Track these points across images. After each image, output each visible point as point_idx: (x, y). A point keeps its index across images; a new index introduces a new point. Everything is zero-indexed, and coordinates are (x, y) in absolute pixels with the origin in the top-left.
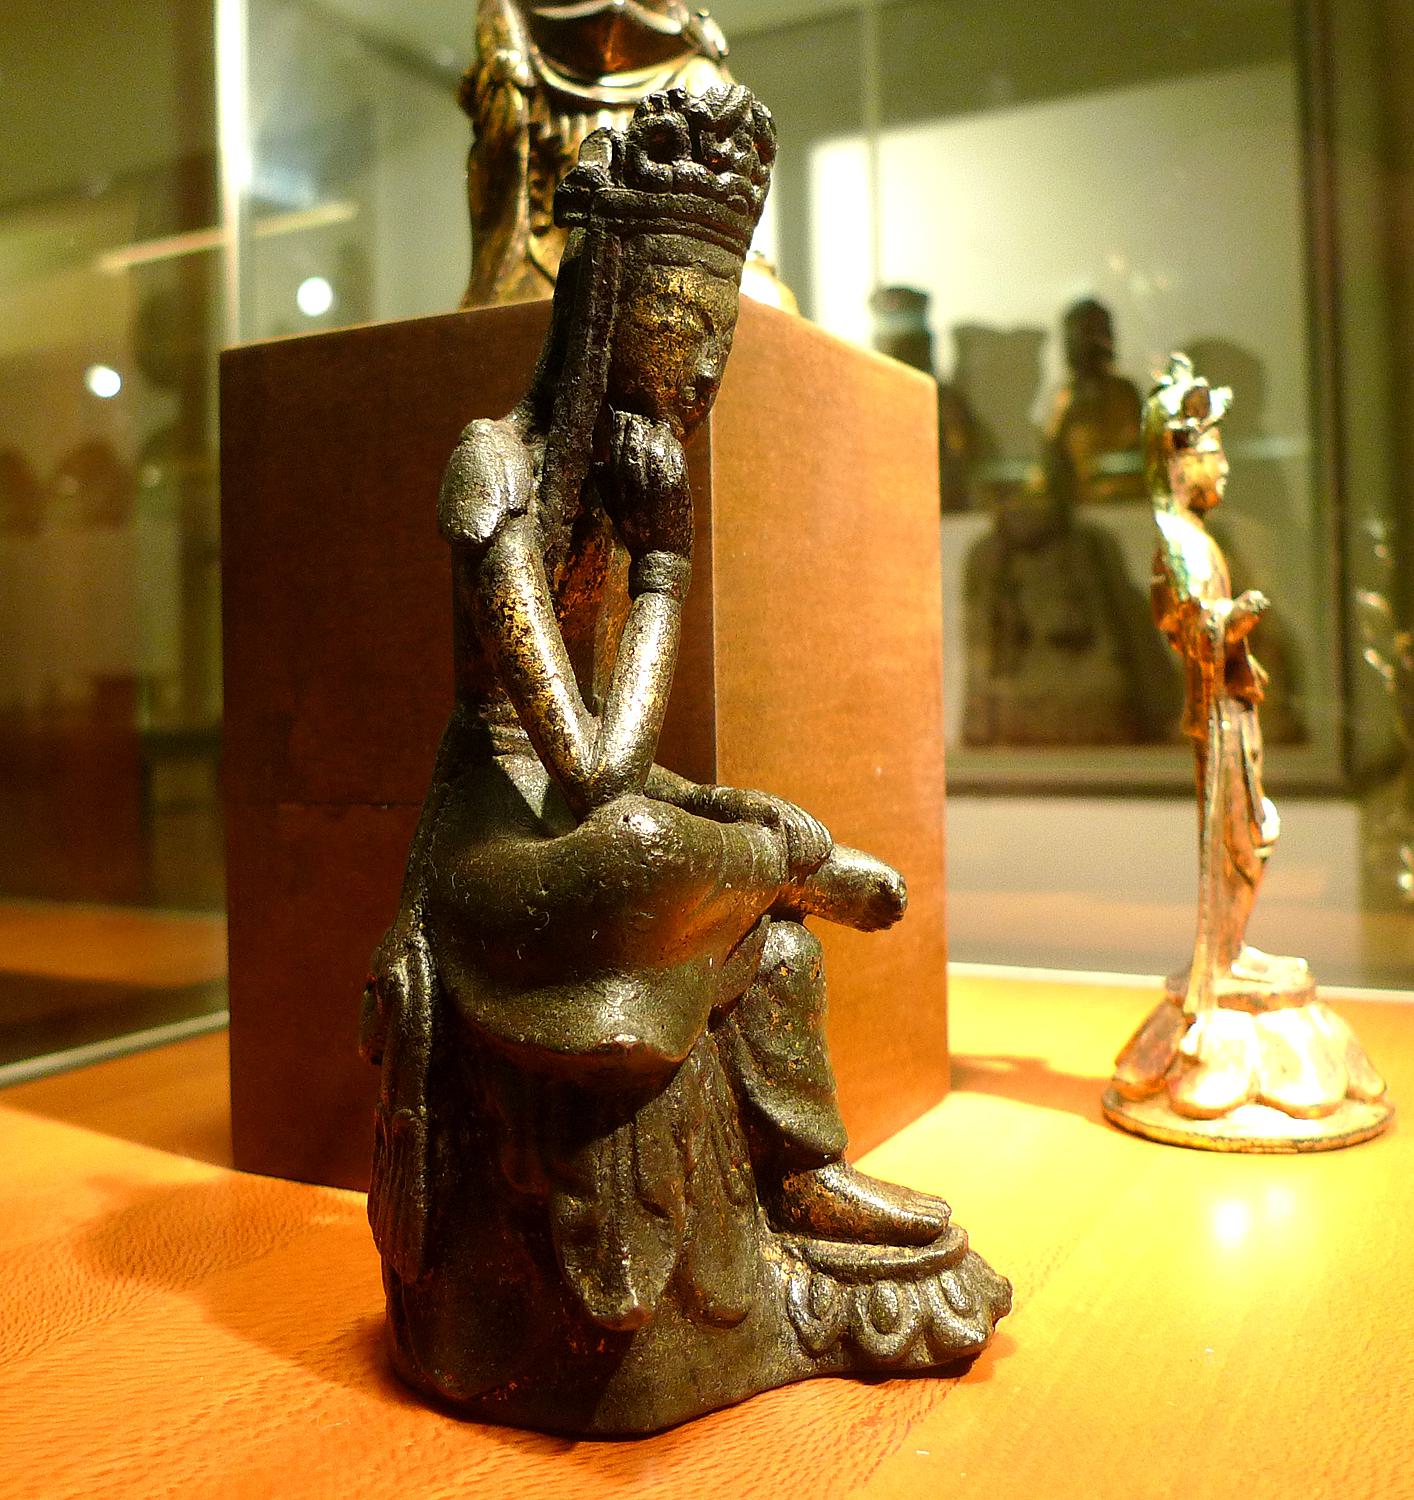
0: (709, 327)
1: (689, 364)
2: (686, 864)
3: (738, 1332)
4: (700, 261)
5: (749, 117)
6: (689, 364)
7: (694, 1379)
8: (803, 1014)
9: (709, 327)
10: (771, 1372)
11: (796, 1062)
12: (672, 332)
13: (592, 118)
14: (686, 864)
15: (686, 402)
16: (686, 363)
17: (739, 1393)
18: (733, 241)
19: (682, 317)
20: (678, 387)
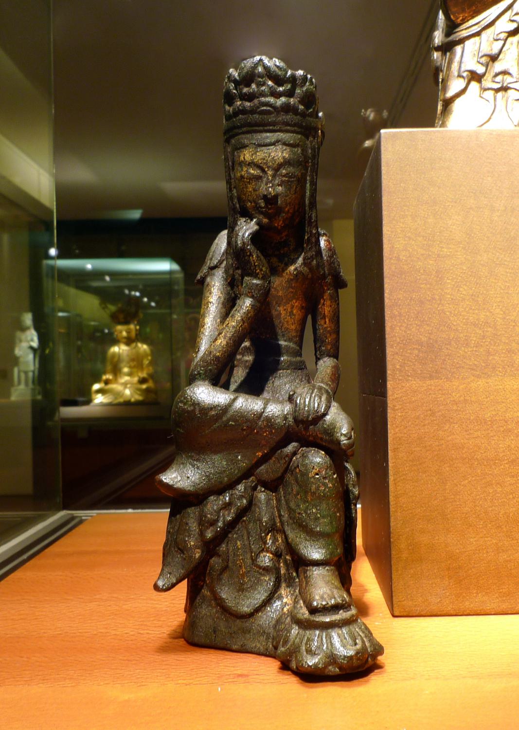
0: (263, 170)
1: (256, 190)
2: (194, 411)
3: (242, 622)
4: (252, 143)
5: (260, 69)
6: (256, 190)
7: (215, 632)
8: (305, 492)
9: (263, 170)
10: (256, 647)
11: (299, 514)
12: (244, 178)
13: (451, 52)
14: (194, 411)
15: (262, 208)
16: (255, 190)
17: (235, 647)
18: (271, 128)
19: (247, 171)
20: (255, 202)
